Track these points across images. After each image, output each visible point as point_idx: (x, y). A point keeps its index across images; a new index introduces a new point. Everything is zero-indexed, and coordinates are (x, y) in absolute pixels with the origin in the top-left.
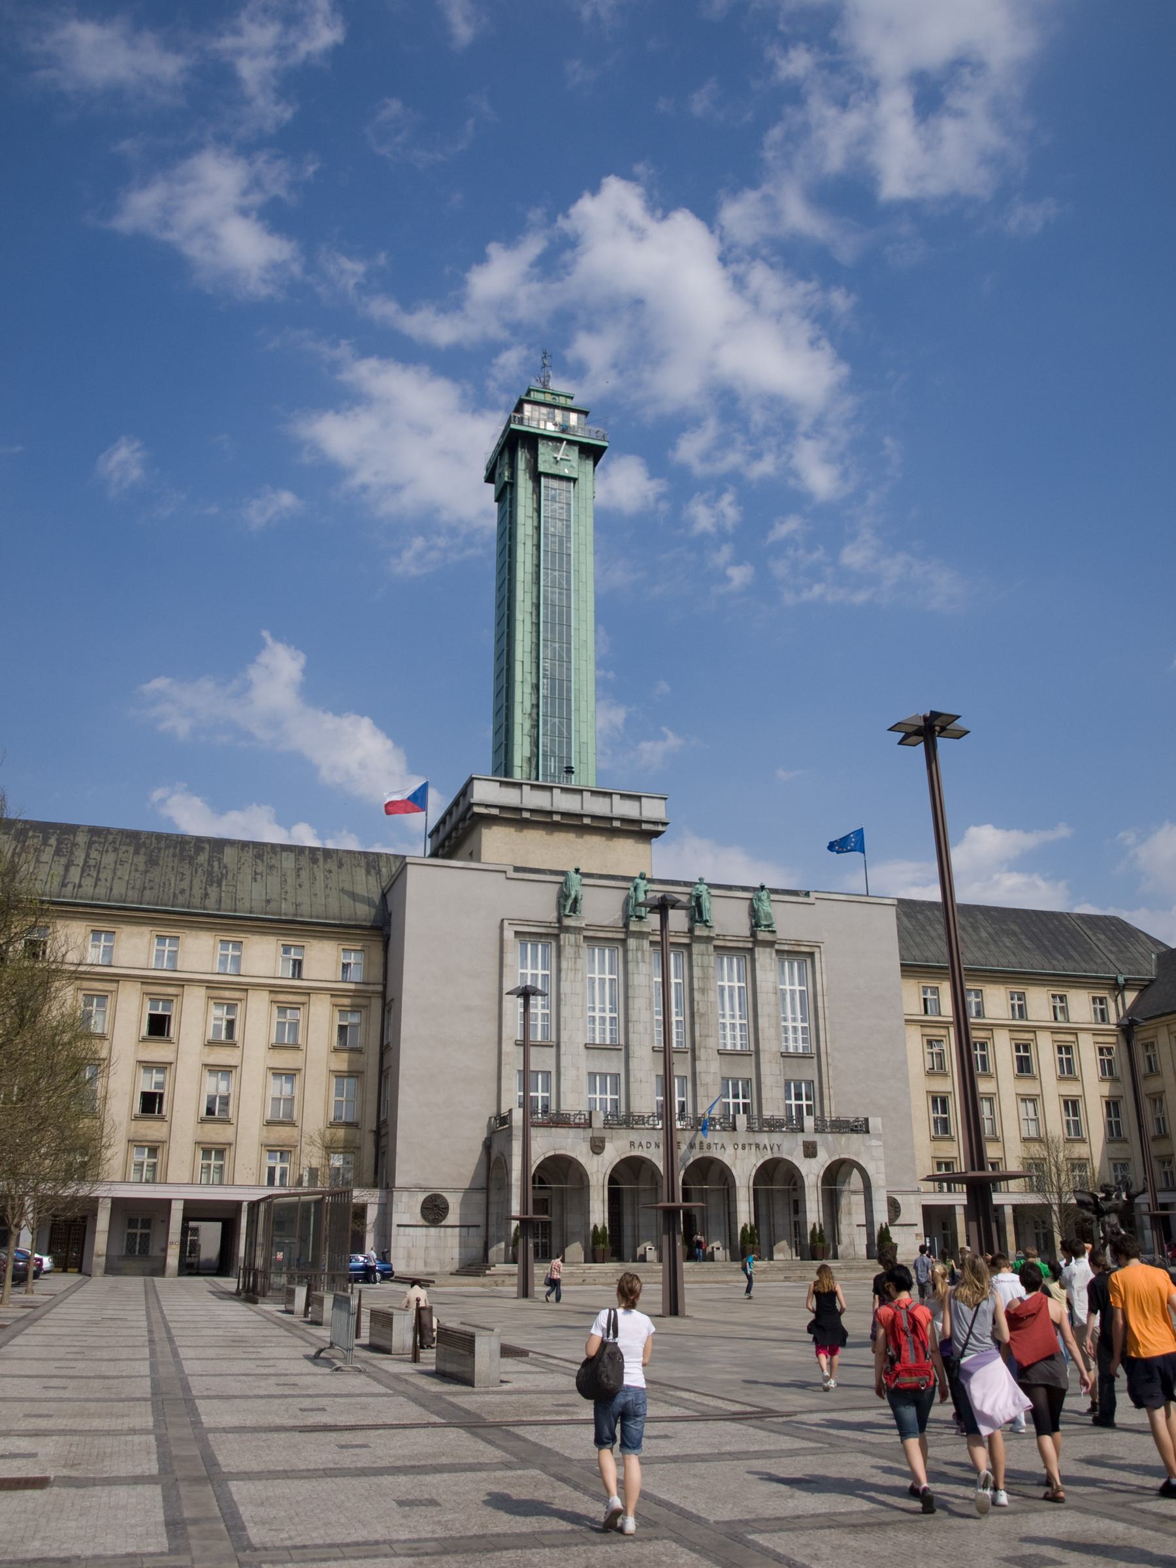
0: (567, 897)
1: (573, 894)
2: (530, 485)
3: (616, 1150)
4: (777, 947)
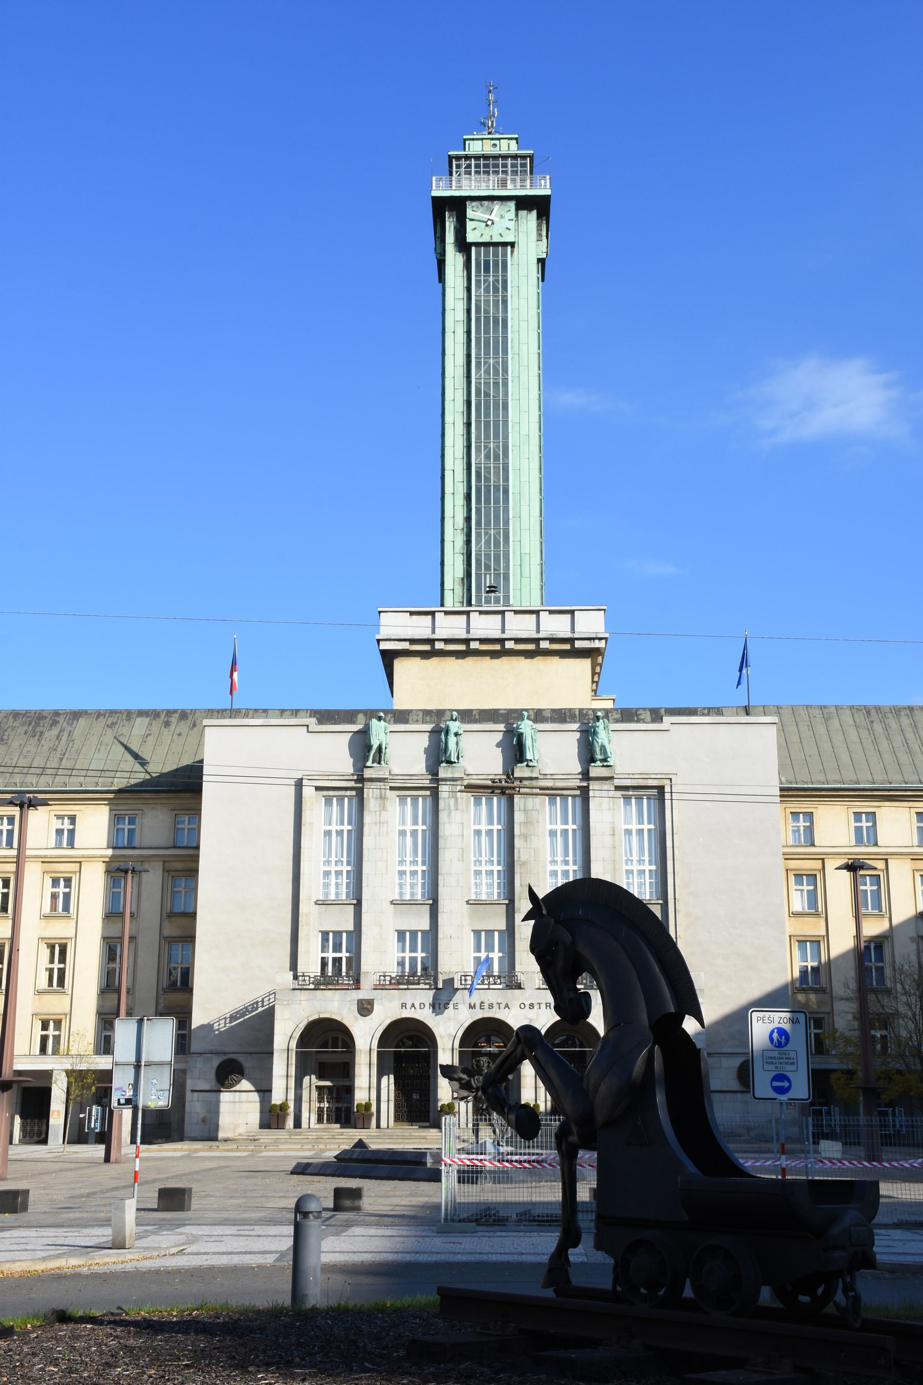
0: (369, 747)
1: (375, 744)
2: (460, 259)
4: (617, 782)
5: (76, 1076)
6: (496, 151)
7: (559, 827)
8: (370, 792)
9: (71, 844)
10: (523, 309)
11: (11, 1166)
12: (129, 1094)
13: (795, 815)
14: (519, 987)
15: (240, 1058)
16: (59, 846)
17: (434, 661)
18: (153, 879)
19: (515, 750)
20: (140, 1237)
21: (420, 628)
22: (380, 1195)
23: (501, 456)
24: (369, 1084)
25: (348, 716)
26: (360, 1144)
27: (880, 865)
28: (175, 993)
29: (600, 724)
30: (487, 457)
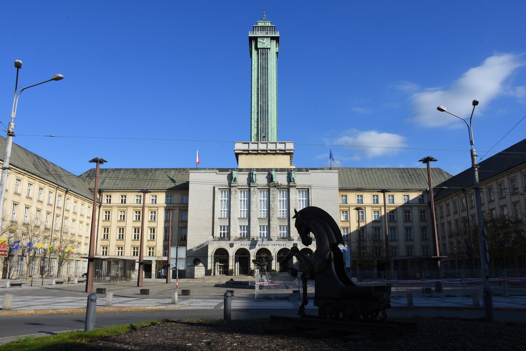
0: (232, 178)
2: (256, 52)
3: (238, 246)
5: (158, 262)
6: (265, 25)
7: (282, 199)
8: (233, 189)
9: (156, 203)
10: (272, 65)
11: (144, 284)
12: (175, 266)
13: (342, 196)
14: (271, 240)
15: (199, 258)
16: (152, 203)
17: (249, 156)
18: (176, 212)
19: (270, 178)
20: (179, 301)
21: (245, 147)
22: (239, 292)
23: (266, 103)
24: (232, 264)
25: (227, 170)
26: (232, 279)
27: (364, 208)
28: (183, 241)
29: (293, 172)
30: (263, 102)
